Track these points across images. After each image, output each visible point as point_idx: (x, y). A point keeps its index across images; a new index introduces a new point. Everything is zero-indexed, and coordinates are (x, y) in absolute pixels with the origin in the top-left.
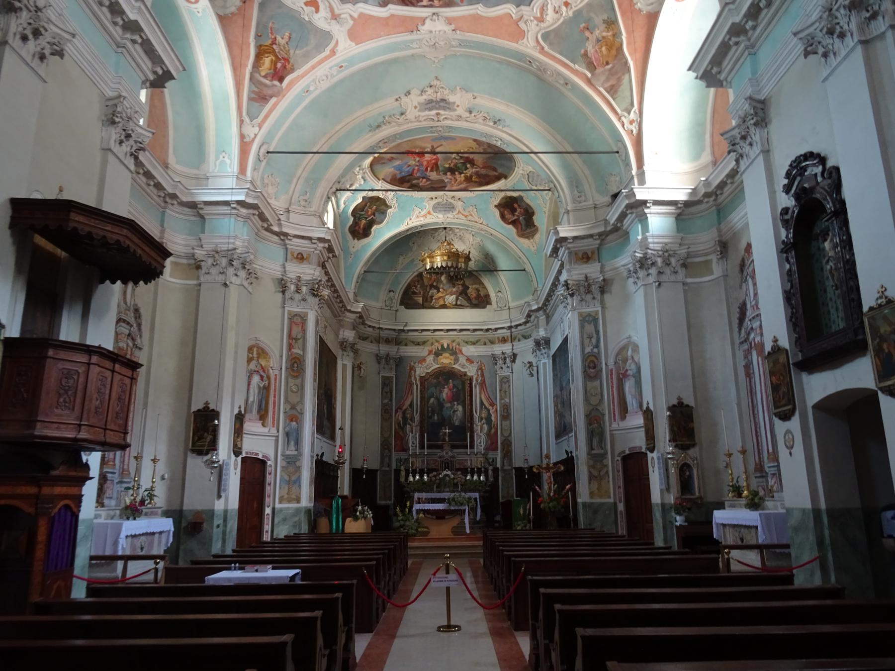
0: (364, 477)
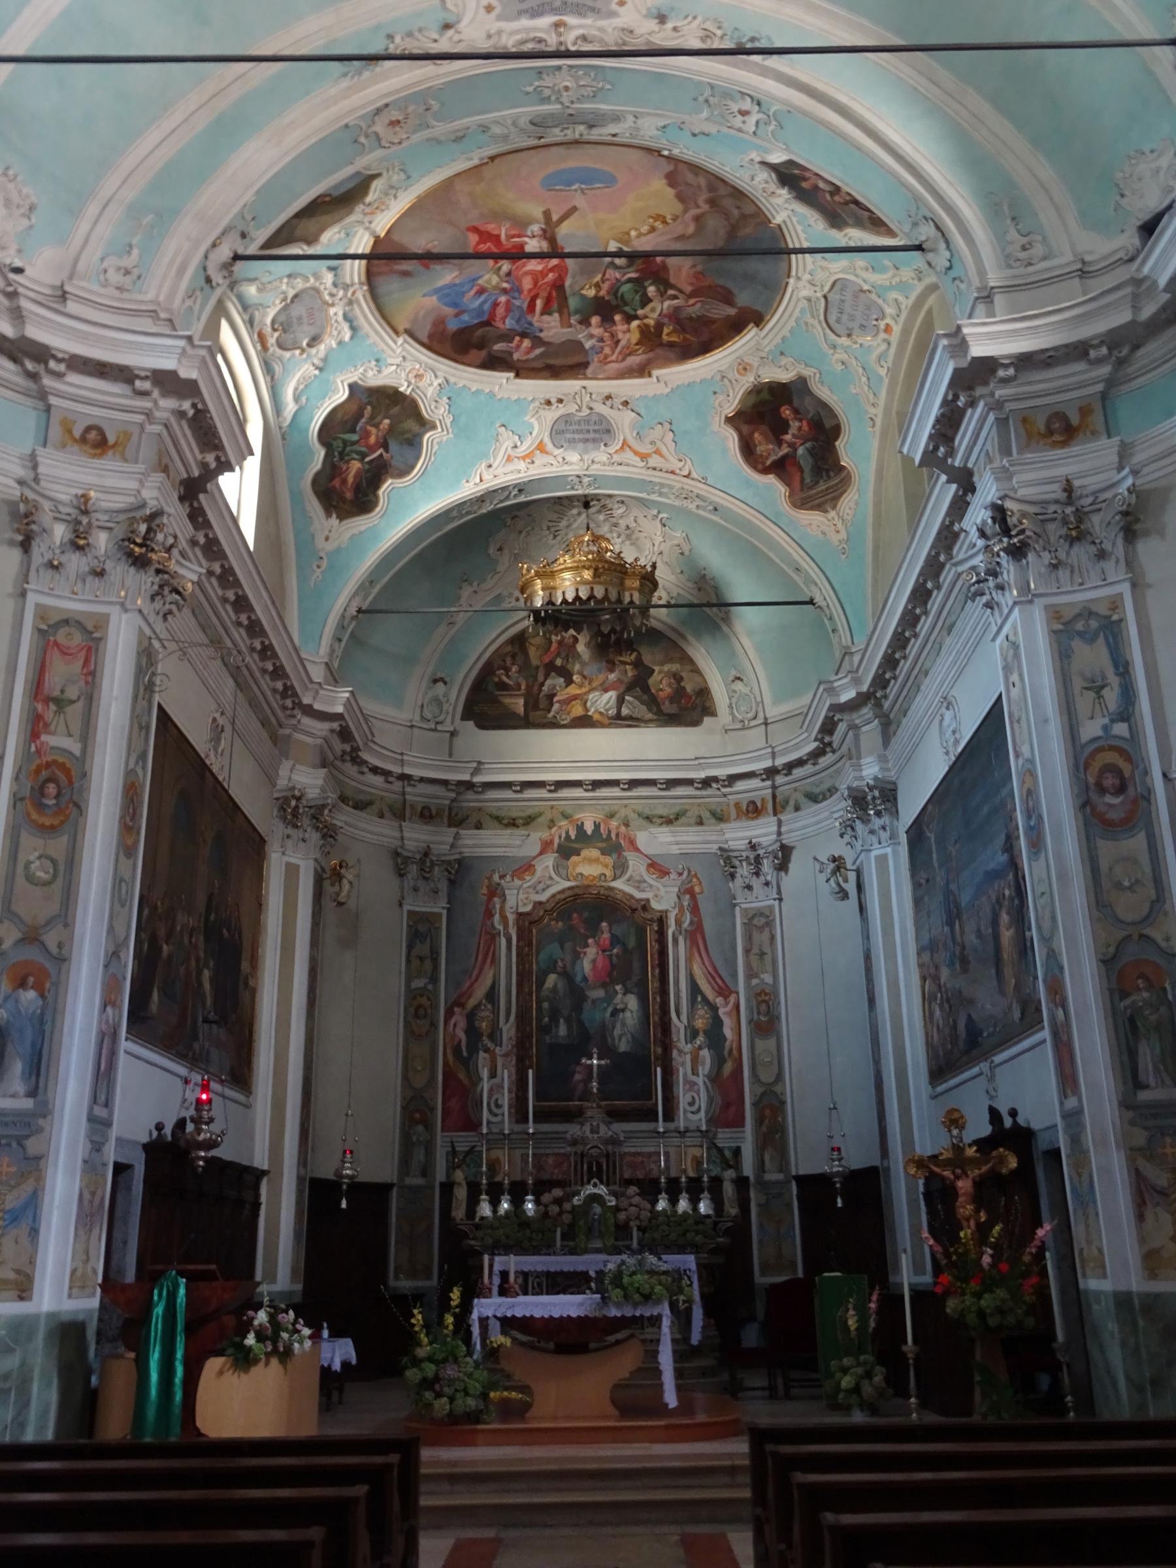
0: (344, 1205)
